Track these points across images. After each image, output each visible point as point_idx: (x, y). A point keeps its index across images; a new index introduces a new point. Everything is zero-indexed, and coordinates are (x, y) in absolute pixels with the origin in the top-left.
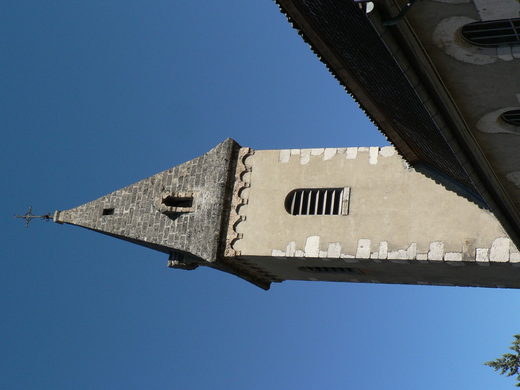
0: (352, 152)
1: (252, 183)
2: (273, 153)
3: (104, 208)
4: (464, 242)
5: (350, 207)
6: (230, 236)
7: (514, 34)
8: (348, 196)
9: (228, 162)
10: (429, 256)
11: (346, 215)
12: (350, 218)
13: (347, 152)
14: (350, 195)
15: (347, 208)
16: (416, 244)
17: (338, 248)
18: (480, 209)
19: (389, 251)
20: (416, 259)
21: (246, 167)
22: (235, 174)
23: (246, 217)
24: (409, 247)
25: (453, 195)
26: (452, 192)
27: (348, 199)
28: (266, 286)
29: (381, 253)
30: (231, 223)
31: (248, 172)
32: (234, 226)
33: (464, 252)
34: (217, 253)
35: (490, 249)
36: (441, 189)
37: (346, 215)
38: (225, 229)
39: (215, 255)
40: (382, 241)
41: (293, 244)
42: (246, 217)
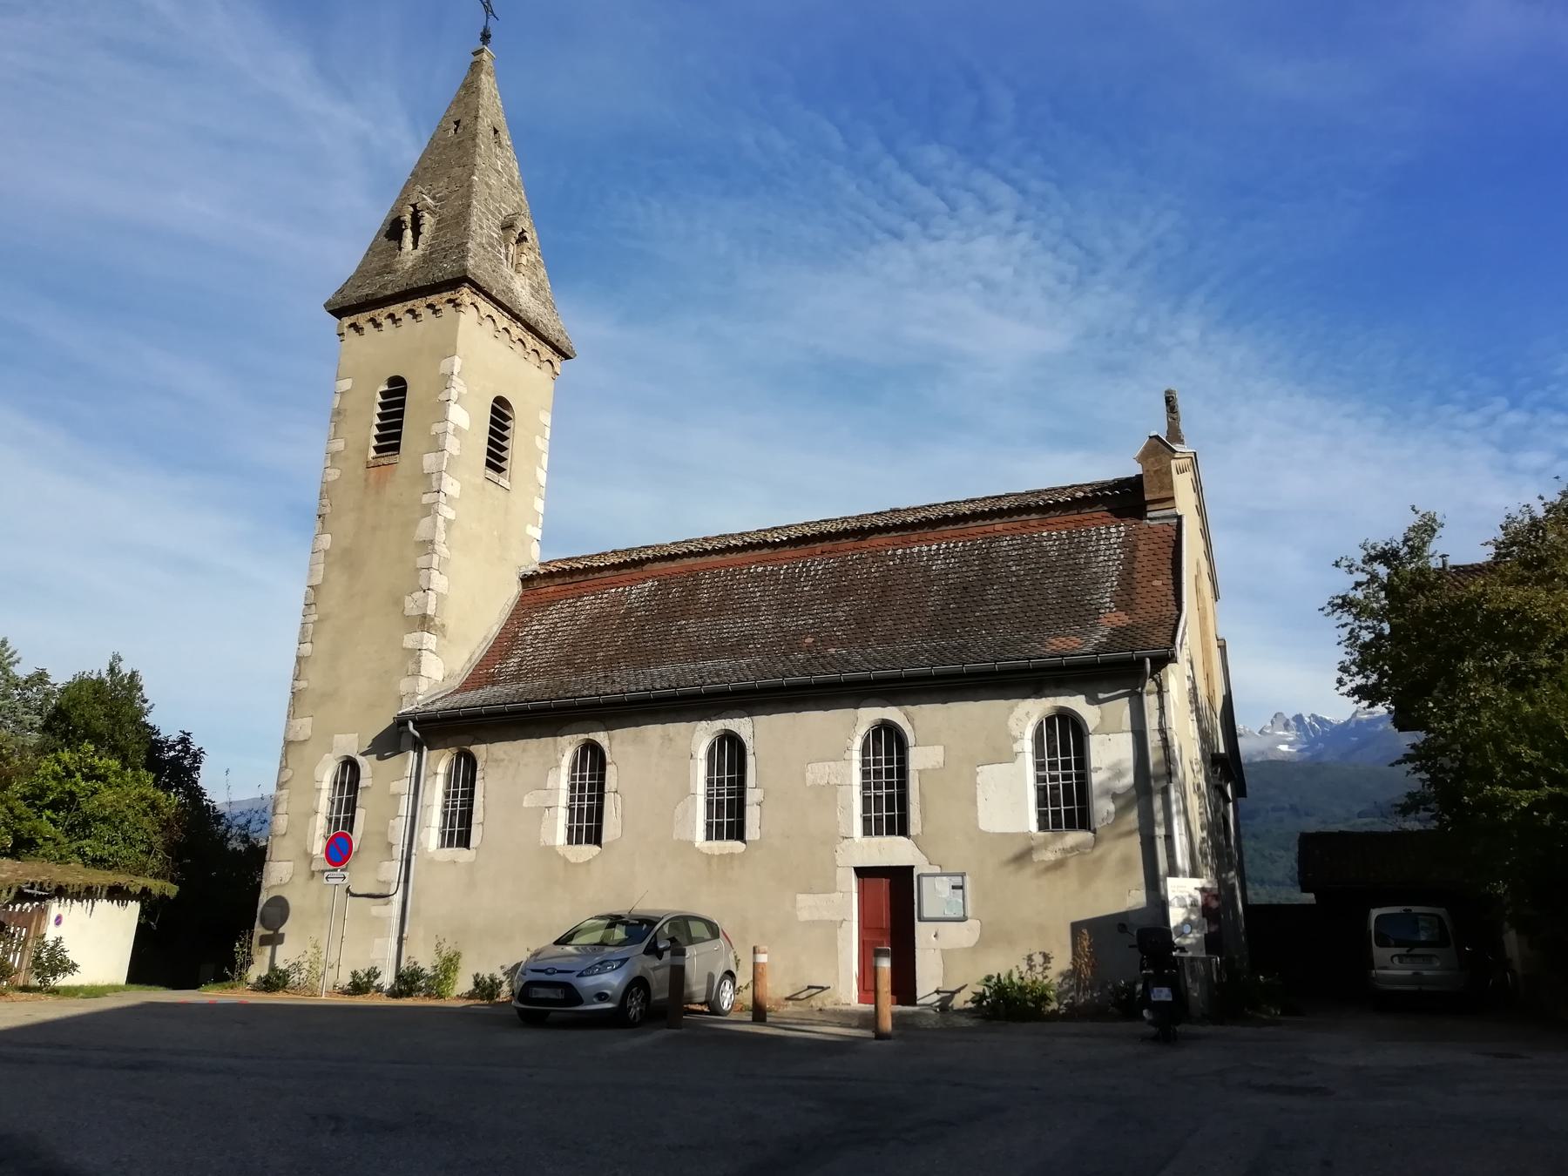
2: (549, 402)
6: (486, 307)
12: (480, 480)
17: (456, 452)
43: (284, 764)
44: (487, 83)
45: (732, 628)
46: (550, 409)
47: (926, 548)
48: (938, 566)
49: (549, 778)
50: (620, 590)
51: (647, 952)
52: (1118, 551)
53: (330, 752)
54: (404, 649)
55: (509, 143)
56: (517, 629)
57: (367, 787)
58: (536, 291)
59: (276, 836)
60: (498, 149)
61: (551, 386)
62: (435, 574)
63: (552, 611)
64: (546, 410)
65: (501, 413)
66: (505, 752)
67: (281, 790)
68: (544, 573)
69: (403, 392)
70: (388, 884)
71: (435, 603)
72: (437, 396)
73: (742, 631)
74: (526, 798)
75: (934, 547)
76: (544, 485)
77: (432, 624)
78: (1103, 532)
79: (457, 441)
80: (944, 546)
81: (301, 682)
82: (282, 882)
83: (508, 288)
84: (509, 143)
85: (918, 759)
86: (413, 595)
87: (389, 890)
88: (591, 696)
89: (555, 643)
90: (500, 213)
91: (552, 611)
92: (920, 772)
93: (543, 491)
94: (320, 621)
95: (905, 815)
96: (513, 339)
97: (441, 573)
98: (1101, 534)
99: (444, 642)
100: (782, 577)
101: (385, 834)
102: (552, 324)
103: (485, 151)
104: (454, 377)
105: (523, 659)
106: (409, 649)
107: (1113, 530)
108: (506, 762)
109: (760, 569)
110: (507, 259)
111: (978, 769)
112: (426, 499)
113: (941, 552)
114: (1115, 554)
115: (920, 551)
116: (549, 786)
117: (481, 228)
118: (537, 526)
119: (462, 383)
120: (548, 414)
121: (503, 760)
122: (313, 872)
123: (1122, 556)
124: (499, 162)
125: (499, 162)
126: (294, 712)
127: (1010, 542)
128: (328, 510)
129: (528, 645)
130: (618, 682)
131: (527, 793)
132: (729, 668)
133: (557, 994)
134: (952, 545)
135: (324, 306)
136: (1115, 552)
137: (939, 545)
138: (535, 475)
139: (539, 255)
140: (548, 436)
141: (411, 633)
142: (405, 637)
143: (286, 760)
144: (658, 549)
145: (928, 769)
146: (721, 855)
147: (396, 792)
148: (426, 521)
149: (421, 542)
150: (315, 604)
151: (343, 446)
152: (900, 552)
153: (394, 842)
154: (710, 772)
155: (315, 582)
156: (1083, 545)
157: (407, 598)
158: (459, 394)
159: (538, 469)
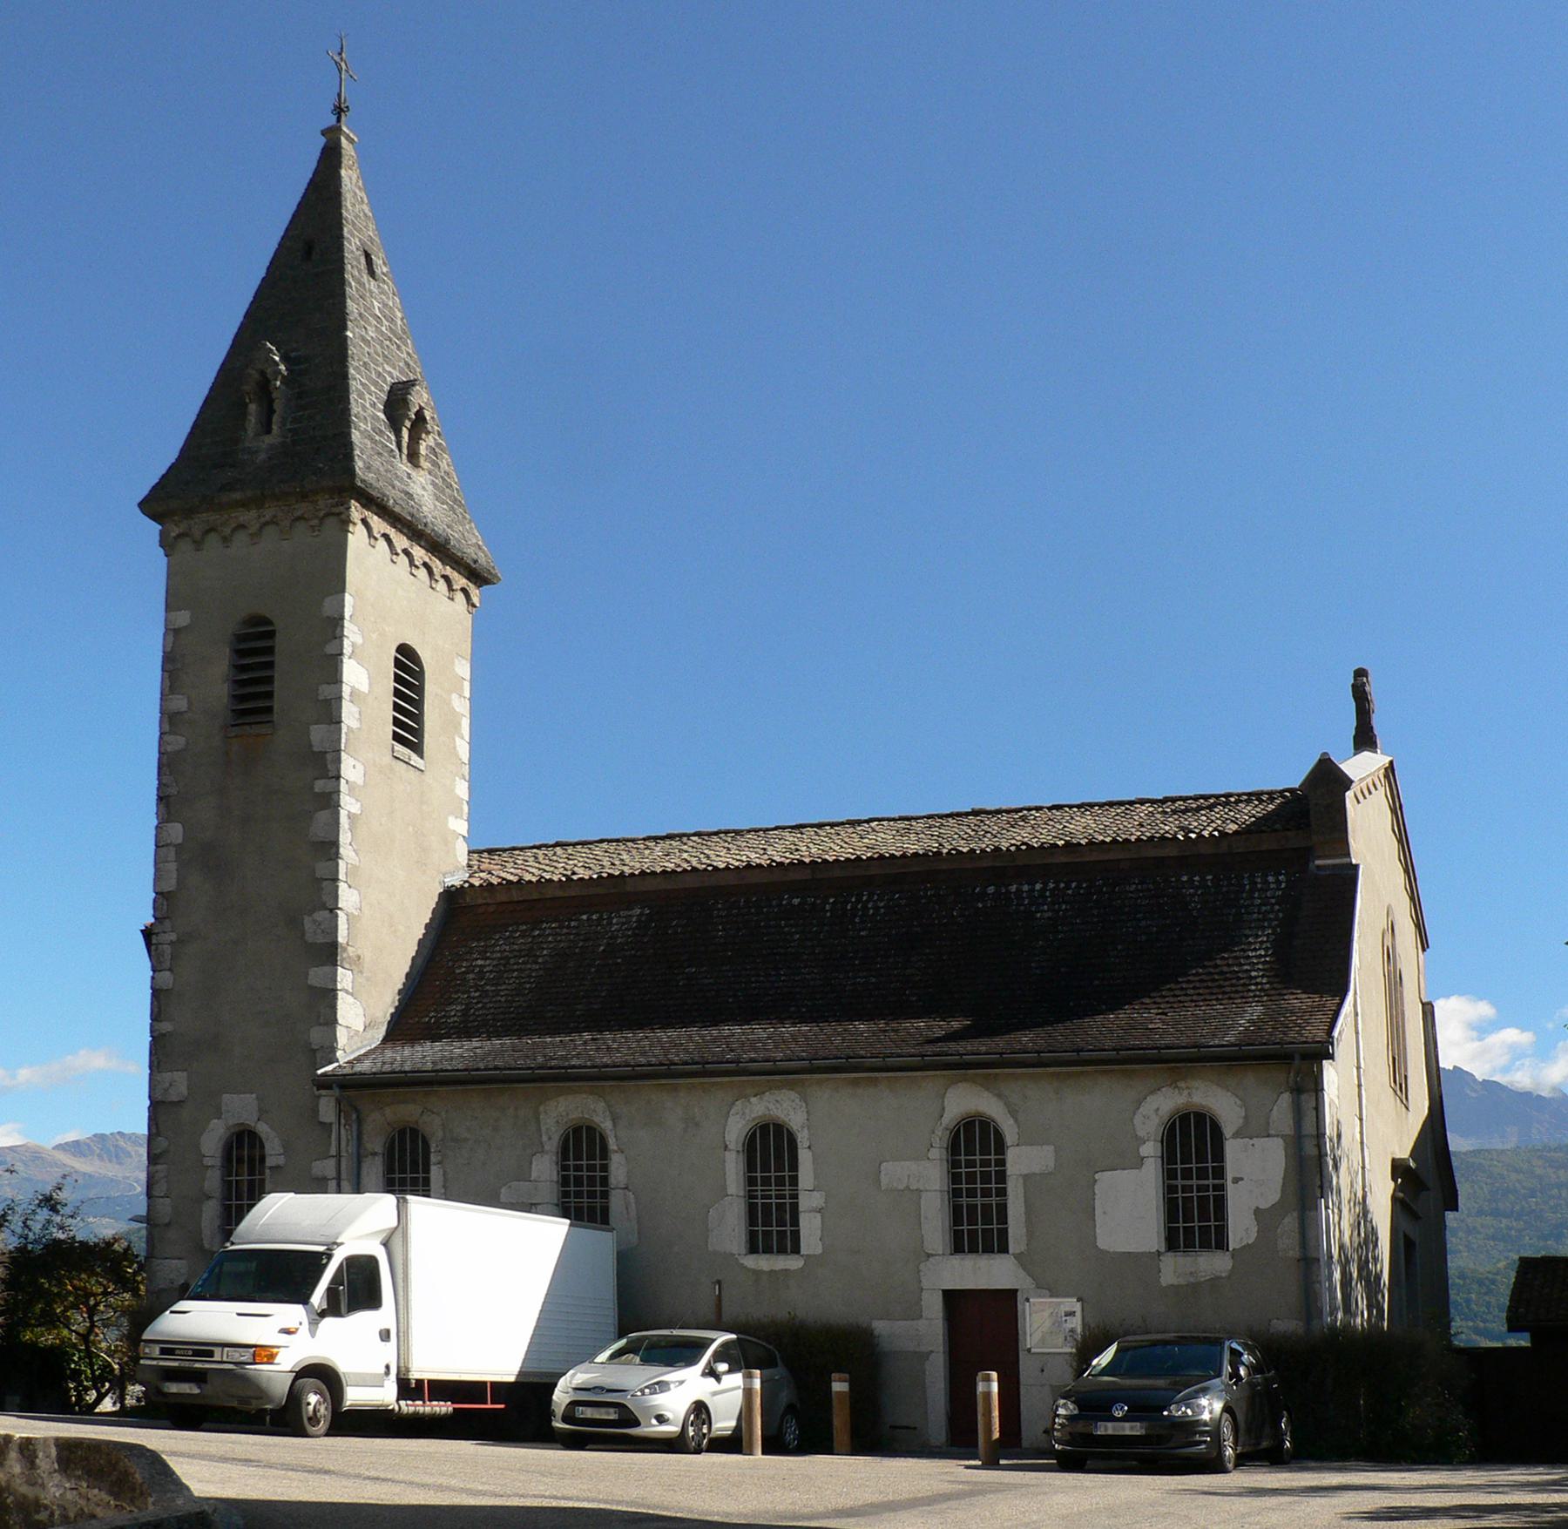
0: (462, 789)
1: (434, 593)
2: (467, 647)
3: (1505, 1328)
4: (359, 952)
5: (402, 763)
6: (378, 524)
7: (349, 1304)
8: (414, 764)
9: (472, 564)
10: (545, 842)
11: (393, 752)
12: (388, 758)
13: (463, 781)
14: (415, 767)
15: (402, 758)
16: (358, 864)
18: (397, 991)
19: (350, 816)
20: (340, 858)
21: (456, 590)
22: (451, 567)
23: (395, 563)
24: (354, 850)
25: (412, 949)
26: (416, 948)
27: (412, 763)
28: (154, 505)
29: (348, 797)
30: (392, 532)
31: (449, 591)
32: (388, 536)
33: (349, 948)
34: (364, 490)
35: (352, 994)
36: (420, 932)
37: (393, 752)
38: (386, 517)
39: (363, 486)
40: (362, 805)
41: (359, 640)
42: (395, 563)
43: (154, 1131)
44: (350, 177)
45: (763, 982)
46: (469, 657)
47: (1026, 888)
48: (1044, 913)
49: (533, 1166)
50: (594, 917)
51: (704, 1374)
52: (1277, 907)
53: (219, 1118)
54: (311, 987)
55: (385, 270)
56: (450, 964)
57: (278, 1167)
58: (441, 488)
60: (373, 282)
61: (467, 620)
62: (342, 887)
63: (498, 940)
64: (463, 658)
65: (408, 665)
67: (156, 1164)
68: (481, 885)
69: (271, 635)
71: (346, 926)
73: (778, 988)
74: (503, 1190)
75: (1038, 886)
76: (467, 762)
77: (345, 955)
78: (1259, 880)
79: (355, 709)
80: (1051, 885)
83: (407, 493)
84: (385, 270)
85: (1022, 1161)
88: (585, 1067)
89: (509, 987)
90: (385, 381)
91: (498, 940)
92: (1027, 1178)
93: (466, 770)
94: (180, 942)
96: (417, 563)
97: (350, 887)
98: (1256, 883)
99: (360, 979)
100: (828, 914)
102: (470, 540)
103: (357, 290)
104: (346, 623)
105: (468, 1007)
107: (1271, 879)
109: (796, 901)
110: (400, 450)
111: (1097, 1176)
112: (319, 786)
113: (1048, 894)
114: (1272, 911)
115: (1019, 891)
116: (534, 1175)
117: (364, 407)
118: (461, 818)
119: (356, 629)
120: (464, 662)
123: (1281, 915)
124: (376, 303)
125: (376, 303)
127: (1139, 887)
129: (471, 987)
130: (617, 1049)
131: (504, 1185)
132: (769, 1038)
133: (612, 1415)
134: (1062, 885)
135: (141, 505)
136: (1268, 938)
137: (1045, 884)
138: (455, 748)
139: (439, 434)
140: (467, 694)
143: (157, 1124)
145: (1035, 1174)
146: (772, 1271)
147: (320, 1174)
148: (323, 816)
151: (186, 706)
152: (991, 889)
154: (750, 1166)
155: (170, 885)
156: (1232, 896)
157: (307, 920)
158: (353, 645)
159: (457, 739)
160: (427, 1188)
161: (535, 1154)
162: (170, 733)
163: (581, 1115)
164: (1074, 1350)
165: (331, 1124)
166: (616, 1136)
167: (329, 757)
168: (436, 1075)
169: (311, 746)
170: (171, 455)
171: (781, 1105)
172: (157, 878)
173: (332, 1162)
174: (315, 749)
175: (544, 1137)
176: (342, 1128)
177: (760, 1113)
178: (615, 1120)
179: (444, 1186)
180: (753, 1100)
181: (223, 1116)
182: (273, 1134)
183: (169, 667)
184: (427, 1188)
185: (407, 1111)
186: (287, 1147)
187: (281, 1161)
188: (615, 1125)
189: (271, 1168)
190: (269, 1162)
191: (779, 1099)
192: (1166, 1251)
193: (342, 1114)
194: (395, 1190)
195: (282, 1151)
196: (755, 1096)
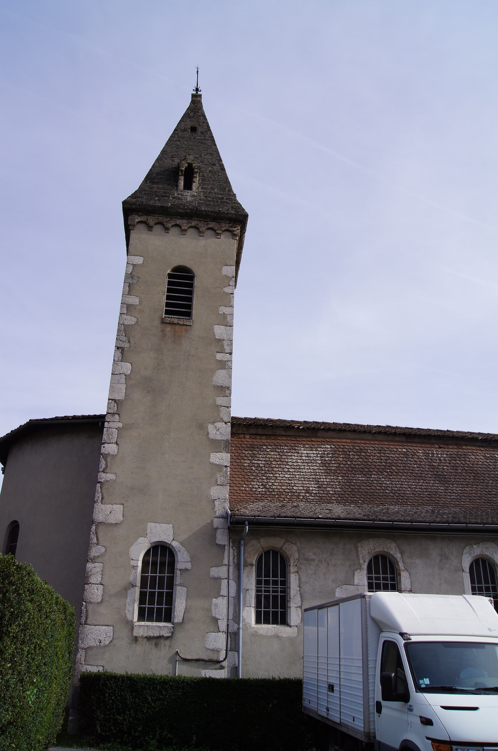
49: (356, 577)
54: (212, 464)
57: (186, 570)
59: (91, 603)
66: (314, 554)
70: (218, 651)
72: (221, 288)
74: (338, 590)
81: (108, 475)
82: (102, 644)
86: (216, 424)
87: (219, 656)
95: (171, 608)
101: (209, 610)
106: (216, 464)
108: (316, 561)
112: (219, 356)
116: (356, 582)
121: (313, 560)
122: (136, 637)
126: (102, 498)
128: (126, 345)
131: (338, 587)
141: (217, 452)
142: (212, 455)
144: (359, 427)
149: (218, 387)
150: (119, 414)
153: (218, 616)
154: (472, 582)
160: (258, 589)
161: (356, 570)
162: (127, 314)
163: (382, 550)
164: (241, 677)
165: (224, 546)
166: (403, 562)
167: (225, 343)
168: (430, 525)
169: (214, 336)
170: (136, 188)
171: (489, 550)
172: (112, 389)
173: (225, 568)
174: (217, 337)
175: (361, 560)
176: (230, 548)
177: (478, 554)
178: (402, 553)
179: (299, 586)
180: (475, 546)
181: (148, 536)
182: (183, 549)
183: (130, 281)
184: (258, 589)
185: (276, 543)
186: (193, 559)
187: (189, 566)
188: (402, 557)
189: (180, 570)
190: (179, 565)
191: (487, 547)
192: (137, 621)
193: (231, 540)
194: (483, 594)
195: (189, 560)
196: (475, 545)
